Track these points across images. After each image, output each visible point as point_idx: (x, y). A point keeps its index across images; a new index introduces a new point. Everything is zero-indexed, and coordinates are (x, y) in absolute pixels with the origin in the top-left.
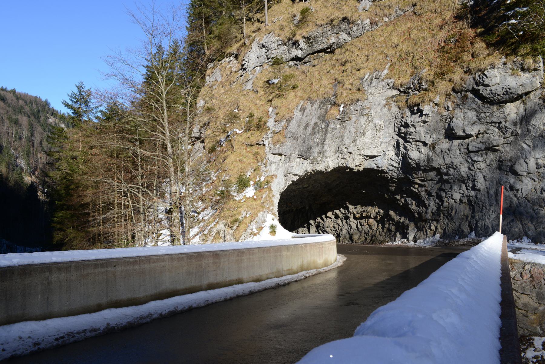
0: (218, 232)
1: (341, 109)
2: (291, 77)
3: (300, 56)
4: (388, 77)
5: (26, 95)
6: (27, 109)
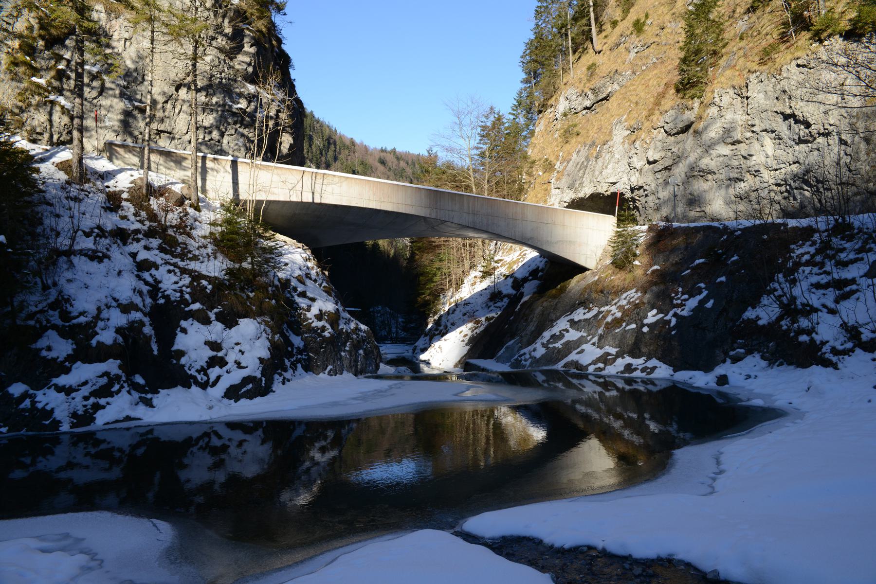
2: (575, 126)
5: (407, 154)
6: (409, 171)
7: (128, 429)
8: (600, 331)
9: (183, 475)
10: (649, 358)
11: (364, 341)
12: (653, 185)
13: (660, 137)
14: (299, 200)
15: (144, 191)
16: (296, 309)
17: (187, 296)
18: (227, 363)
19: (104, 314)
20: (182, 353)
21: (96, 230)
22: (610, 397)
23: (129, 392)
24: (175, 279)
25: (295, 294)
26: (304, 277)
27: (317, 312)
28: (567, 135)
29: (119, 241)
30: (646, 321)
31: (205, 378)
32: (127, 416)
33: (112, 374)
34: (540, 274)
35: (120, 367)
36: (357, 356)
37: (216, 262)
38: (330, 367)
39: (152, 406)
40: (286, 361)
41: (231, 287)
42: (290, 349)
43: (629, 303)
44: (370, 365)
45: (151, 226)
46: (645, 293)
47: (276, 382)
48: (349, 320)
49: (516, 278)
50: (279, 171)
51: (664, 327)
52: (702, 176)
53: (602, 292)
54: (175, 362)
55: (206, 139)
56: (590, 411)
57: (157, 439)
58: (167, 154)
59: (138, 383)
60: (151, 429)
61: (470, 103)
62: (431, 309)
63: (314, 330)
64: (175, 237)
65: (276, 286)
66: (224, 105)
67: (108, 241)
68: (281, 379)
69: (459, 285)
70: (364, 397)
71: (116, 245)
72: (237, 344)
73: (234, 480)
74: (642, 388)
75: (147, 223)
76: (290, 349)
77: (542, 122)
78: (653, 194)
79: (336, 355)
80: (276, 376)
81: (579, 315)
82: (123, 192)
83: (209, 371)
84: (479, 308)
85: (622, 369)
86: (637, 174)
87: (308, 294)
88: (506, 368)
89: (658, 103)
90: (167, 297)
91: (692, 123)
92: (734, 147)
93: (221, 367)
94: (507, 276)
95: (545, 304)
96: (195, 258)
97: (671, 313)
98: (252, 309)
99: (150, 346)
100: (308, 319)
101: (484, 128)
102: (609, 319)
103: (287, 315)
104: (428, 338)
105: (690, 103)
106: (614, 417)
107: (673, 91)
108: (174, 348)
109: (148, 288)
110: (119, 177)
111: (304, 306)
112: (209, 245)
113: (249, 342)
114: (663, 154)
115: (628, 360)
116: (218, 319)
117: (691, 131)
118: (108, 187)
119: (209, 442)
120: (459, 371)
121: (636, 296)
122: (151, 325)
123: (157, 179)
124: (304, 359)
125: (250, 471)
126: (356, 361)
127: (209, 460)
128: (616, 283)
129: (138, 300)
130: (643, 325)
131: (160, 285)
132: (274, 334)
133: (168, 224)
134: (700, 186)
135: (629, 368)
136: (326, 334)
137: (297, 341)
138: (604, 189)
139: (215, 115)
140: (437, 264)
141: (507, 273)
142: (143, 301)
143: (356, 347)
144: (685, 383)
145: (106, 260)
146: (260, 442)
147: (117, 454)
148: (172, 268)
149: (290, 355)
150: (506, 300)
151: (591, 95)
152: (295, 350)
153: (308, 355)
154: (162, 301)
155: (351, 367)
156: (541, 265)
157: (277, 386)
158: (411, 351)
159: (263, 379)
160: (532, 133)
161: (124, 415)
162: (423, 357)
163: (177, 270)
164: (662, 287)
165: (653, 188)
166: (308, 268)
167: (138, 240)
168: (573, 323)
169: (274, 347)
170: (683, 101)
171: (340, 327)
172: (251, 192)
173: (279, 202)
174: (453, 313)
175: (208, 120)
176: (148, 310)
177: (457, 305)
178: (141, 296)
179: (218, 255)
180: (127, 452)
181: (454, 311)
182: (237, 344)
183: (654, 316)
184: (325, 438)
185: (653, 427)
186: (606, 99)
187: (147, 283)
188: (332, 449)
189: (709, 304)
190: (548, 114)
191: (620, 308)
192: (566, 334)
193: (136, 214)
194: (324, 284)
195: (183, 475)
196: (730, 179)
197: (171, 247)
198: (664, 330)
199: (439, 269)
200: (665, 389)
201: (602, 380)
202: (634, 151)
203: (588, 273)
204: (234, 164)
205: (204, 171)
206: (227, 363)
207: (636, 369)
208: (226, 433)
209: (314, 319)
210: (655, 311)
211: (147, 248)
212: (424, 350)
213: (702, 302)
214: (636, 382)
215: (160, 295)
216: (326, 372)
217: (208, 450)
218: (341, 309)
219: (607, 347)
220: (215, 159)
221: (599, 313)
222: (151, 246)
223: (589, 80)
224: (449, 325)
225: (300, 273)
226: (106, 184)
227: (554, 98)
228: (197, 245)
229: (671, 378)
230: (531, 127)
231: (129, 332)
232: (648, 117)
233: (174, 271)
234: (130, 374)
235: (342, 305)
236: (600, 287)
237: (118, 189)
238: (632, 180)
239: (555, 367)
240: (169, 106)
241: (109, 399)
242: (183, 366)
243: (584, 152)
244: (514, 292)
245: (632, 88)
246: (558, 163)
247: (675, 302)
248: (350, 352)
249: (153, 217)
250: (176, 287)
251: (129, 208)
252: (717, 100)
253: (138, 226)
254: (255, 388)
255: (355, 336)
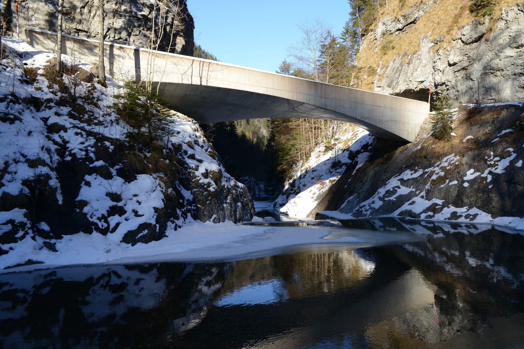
0: (346, 129)
1: (409, 57)
2: (391, 42)
3: (400, 28)
4: (431, 36)
7: (30, 272)
8: (427, 187)
9: (86, 310)
10: (471, 207)
11: (241, 195)
12: (453, 82)
13: (458, 46)
14: (190, 83)
15: (58, 68)
16: (186, 169)
17: (92, 155)
18: (125, 212)
19: (12, 168)
20: (85, 203)
21: (10, 97)
22: (437, 238)
23: (33, 238)
24: (81, 140)
25: (185, 156)
26: (193, 143)
27: (204, 171)
28: (385, 49)
29: (32, 108)
30: (465, 178)
31: (105, 225)
32: (30, 260)
33: (17, 221)
34: (370, 147)
35: (25, 215)
36: (236, 207)
37: (118, 127)
38: (214, 216)
39: (55, 250)
40: (178, 211)
41: (131, 148)
42: (181, 201)
43: (450, 164)
44: (246, 215)
45: (62, 96)
46: (463, 156)
47: (169, 228)
48: (230, 178)
49: (351, 151)
50: (174, 60)
51: (481, 182)
52: (492, 73)
53: (425, 157)
54: (78, 210)
55: (116, 38)
56: (416, 250)
57: (60, 280)
58: (82, 42)
59: (43, 230)
60: (53, 272)
61: (315, 24)
62: (286, 175)
63: (202, 186)
64: (83, 106)
65: (170, 149)
66: (131, 12)
67: (21, 106)
68: (173, 226)
69: (307, 156)
70: (244, 241)
71: (29, 110)
72: (135, 195)
73: (134, 312)
74: (465, 232)
75: (59, 94)
76: (181, 201)
77: (365, 42)
78: (454, 88)
79: (219, 206)
80: (169, 223)
81: (407, 175)
82: (40, 69)
83: (109, 219)
84: (324, 173)
85: (449, 216)
86: (440, 74)
87: (197, 157)
88: (348, 217)
89: (456, 21)
90: (74, 155)
91: (484, 34)
92: (518, 50)
93: (120, 216)
94: (345, 150)
95: (376, 169)
96: (100, 123)
97: (487, 171)
98: (148, 167)
99: (56, 197)
100: (196, 177)
101: (324, 46)
102: (434, 177)
103: (179, 173)
104: (285, 196)
105: (482, 19)
106: (439, 253)
107: (468, 12)
108: (78, 199)
109: (56, 147)
110: (36, 57)
111: (193, 166)
112: (113, 114)
113: (146, 193)
114: (460, 58)
115: (453, 209)
116: (118, 174)
117: (483, 40)
118: (26, 64)
119: (108, 281)
120: (312, 219)
121: (455, 159)
122: (57, 178)
123: (67, 59)
124: (193, 210)
125: (148, 303)
126: (235, 211)
127: (109, 296)
128: (437, 150)
129: (45, 157)
130: (464, 182)
131: (68, 145)
132: (167, 187)
133: (77, 95)
134: (493, 80)
135: (454, 215)
136: (212, 189)
137: (187, 195)
138: (414, 86)
139: (123, 19)
140: (292, 142)
141: (344, 148)
142: (51, 157)
143: (235, 200)
144: (506, 227)
145: (17, 122)
146: (155, 279)
147: (21, 295)
148: (79, 131)
149: (182, 206)
150: (344, 167)
151: (402, 20)
152: (185, 202)
153: (196, 206)
154: (69, 158)
155: (231, 216)
156: (370, 142)
157: (170, 231)
158: (272, 206)
159: (158, 226)
160: (358, 50)
161: (27, 259)
162: (283, 210)
163: (84, 133)
164: (477, 152)
165: (453, 84)
166: (196, 137)
167: (50, 108)
168: (402, 181)
169: (167, 199)
170: (476, 18)
171: (223, 184)
172: (149, 73)
173: (173, 84)
174: (304, 177)
175: (119, 23)
176: (55, 165)
177: (306, 172)
178: (49, 154)
179: (121, 121)
180: (31, 293)
181: (305, 176)
182: (135, 195)
183: (472, 174)
184: (211, 274)
185: (472, 262)
186: (413, 22)
187: (55, 143)
188: (216, 282)
189: (519, 164)
190: (370, 36)
191: (443, 169)
192: (398, 190)
193: (49, 87)
194: (209, 150)
195: (86, 310)
196: (515, 74)
197: (80, 114)
198: (482, 185)
199: (293, 145)
200: (484, 232)
201: (432, 225)
202: (437, 57)
203: (409, 145)
204: (137, 52)
205: (112, 57)
206: (125, 212)
207: (460, 216)
208: (122, 272)
209: (201, 176)
210: (472, 171)
211: (57, 114)
212: (282, 205)
213: (512, 163)
214: (460, 226)
215: (67, 153)
216: (212, 220)
217: (108, 288)
218: (223, 170)
219: (434, 199)
220: (121, 47)
221: (424, 173)
222: (61, 112)
223: (401, 9)
224: (301, 186)
225: (190, 139)
226: (24, 62)
227: (373, 25)
228: (101, 113)
229: (492, 223)
230: (356, 47)
231: (36, 185)
232: (448, 32)
233: (81, 133)
234: (35, 223)
235: (224, 167)
236: (424, 153)
237: (34, 66)
238: (436, 78)
239: (391, 215)
240: (86, 10)
241: (12, 245)
242: (86, 214)
243: (398, 61)
244: (350, 161)
245: (434, 13)
246: (379, 69)
247: (488, 163)
248: (230, 204)
249: (64, 89)
250: (82, 146)
251: (44, 82)
252: (504, 15)
253: (51, 96)
254: (152, 233)
255: (234, 192)
